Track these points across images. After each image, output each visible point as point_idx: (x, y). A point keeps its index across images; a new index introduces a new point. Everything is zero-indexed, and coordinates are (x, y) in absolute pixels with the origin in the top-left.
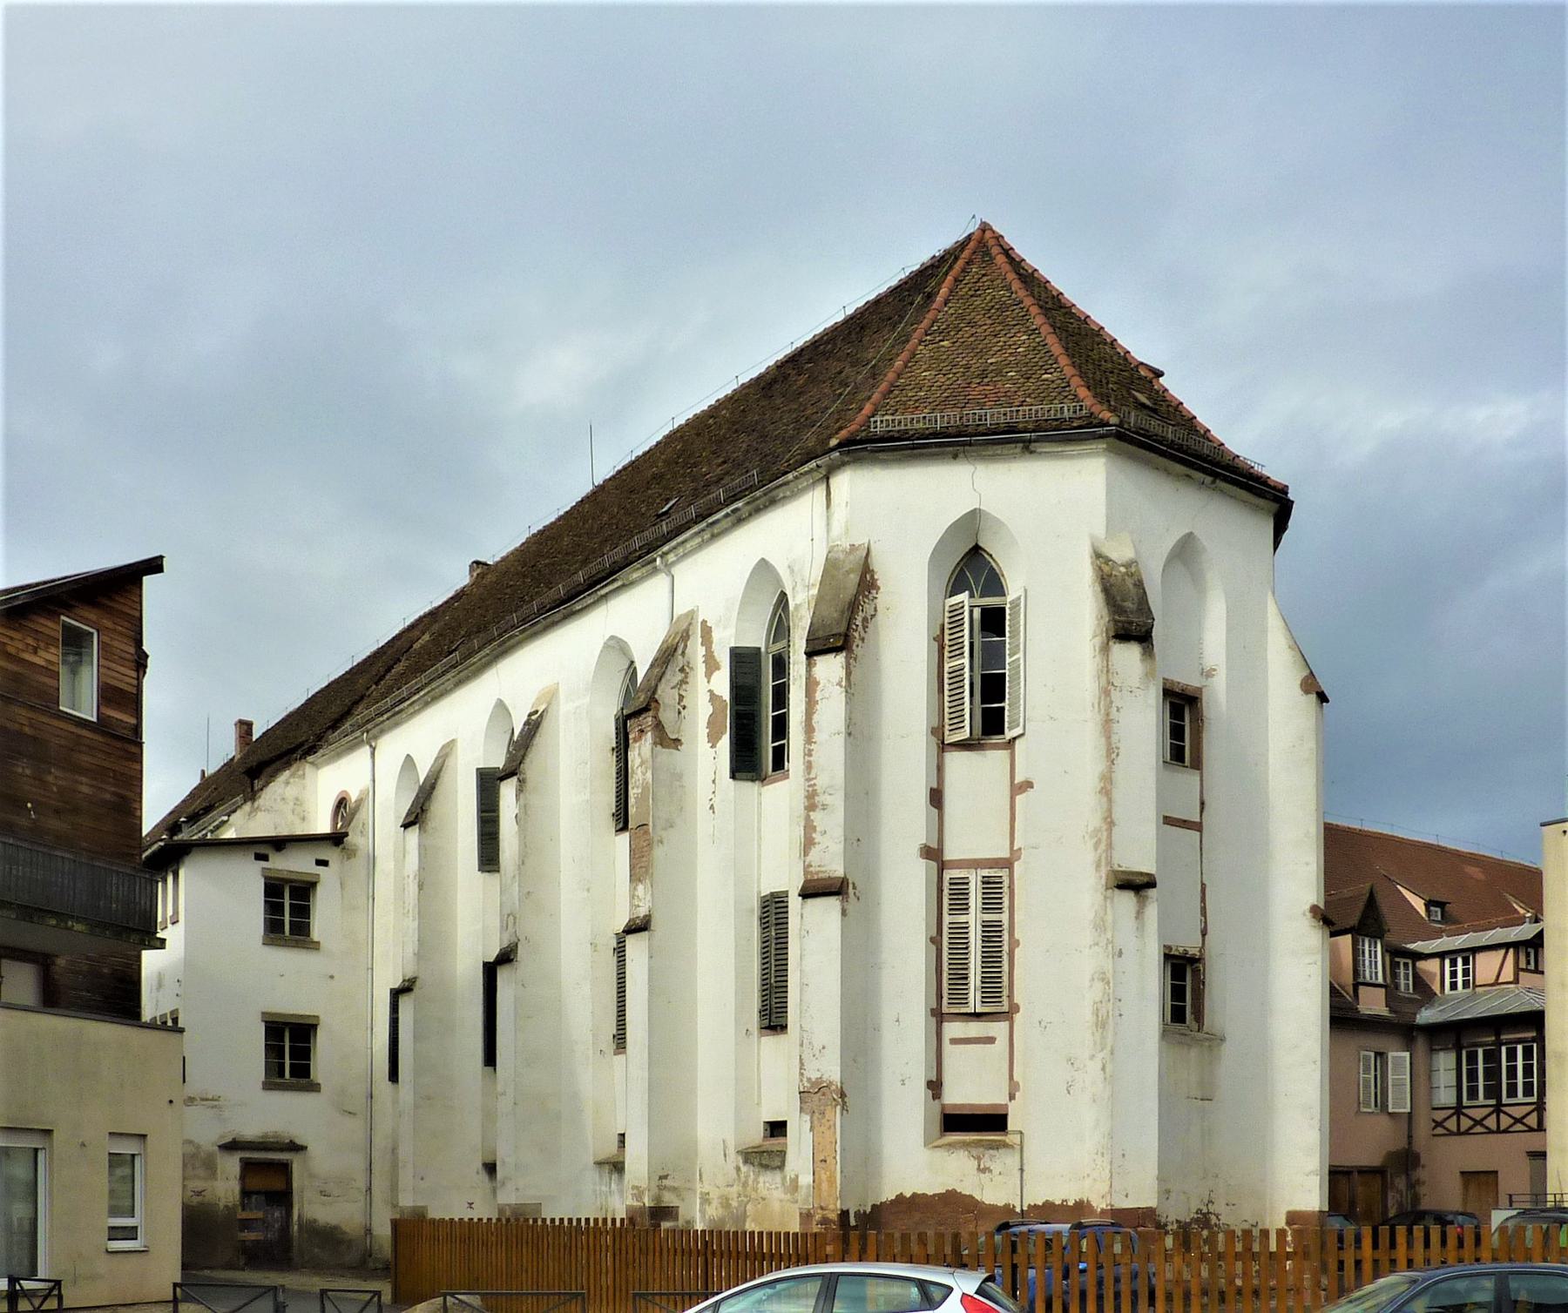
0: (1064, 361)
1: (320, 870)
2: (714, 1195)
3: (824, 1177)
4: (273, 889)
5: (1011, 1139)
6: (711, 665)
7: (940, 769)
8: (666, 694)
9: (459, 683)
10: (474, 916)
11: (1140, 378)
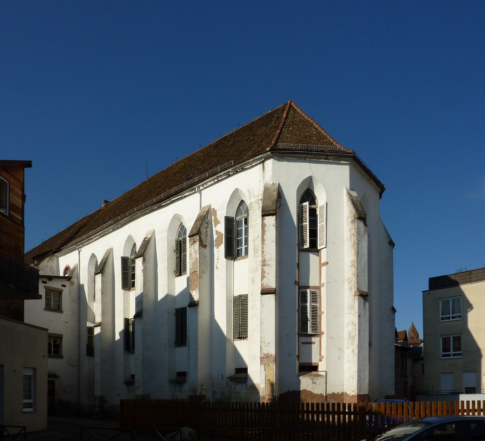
9: (114, 230)
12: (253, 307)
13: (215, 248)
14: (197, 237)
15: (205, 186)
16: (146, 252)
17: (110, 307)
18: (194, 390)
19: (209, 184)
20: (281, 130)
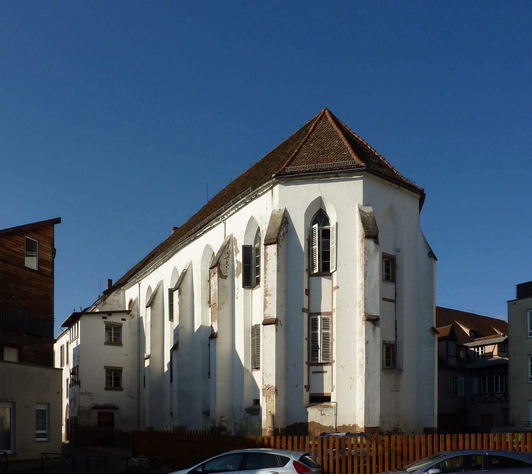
0: (349, 148)
1: (123, 322)
5: (333, 404)
11: (376, 155)
13: (236, 277)
14: (216, 269)
15: (228, 215)
16: (182, 285)
17: (159, 339)
18: (214, 422)
19: (231, 212)
20: (301, 147)
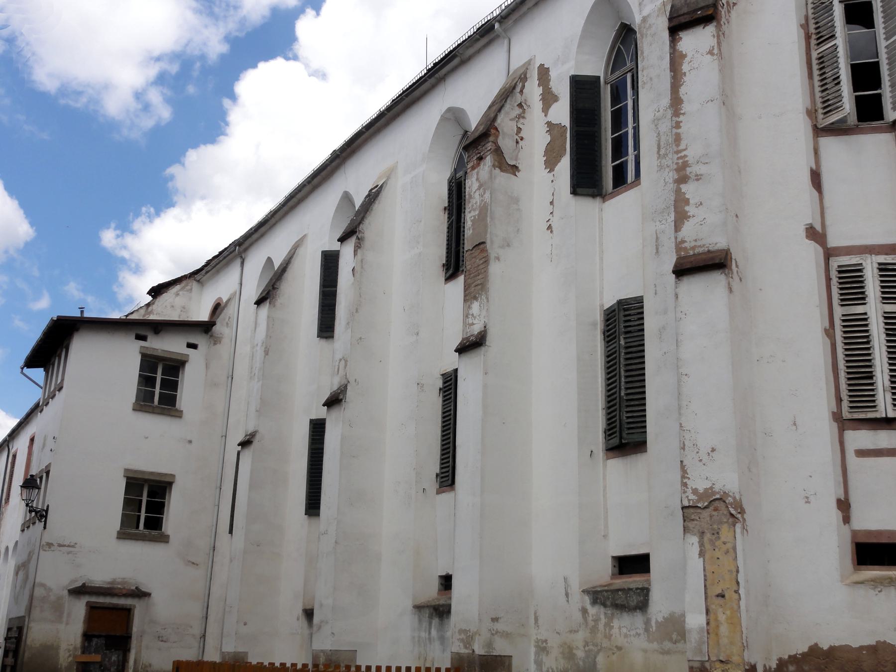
2: (554, 642)
3: (722, 618)
4: (149, 362)
6: (549, 98)
7: (816, 152)
8: (505, 123)
10: (309, 369)
12: (662, 330)
